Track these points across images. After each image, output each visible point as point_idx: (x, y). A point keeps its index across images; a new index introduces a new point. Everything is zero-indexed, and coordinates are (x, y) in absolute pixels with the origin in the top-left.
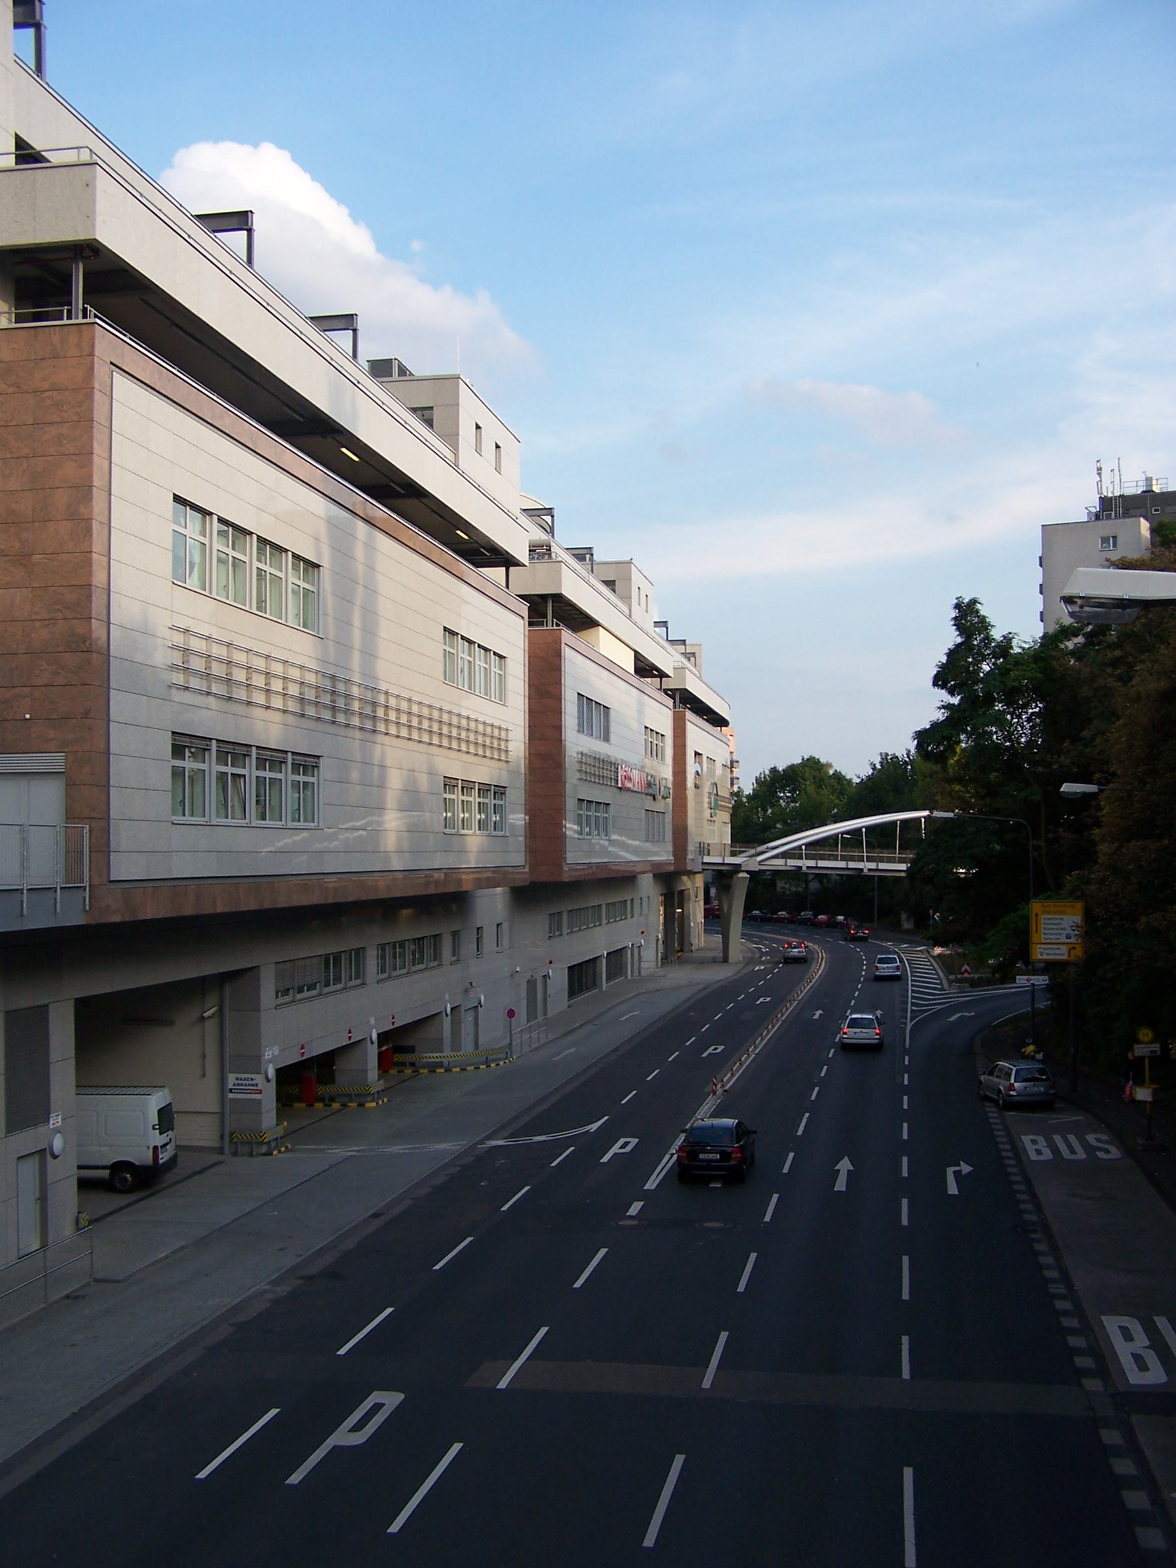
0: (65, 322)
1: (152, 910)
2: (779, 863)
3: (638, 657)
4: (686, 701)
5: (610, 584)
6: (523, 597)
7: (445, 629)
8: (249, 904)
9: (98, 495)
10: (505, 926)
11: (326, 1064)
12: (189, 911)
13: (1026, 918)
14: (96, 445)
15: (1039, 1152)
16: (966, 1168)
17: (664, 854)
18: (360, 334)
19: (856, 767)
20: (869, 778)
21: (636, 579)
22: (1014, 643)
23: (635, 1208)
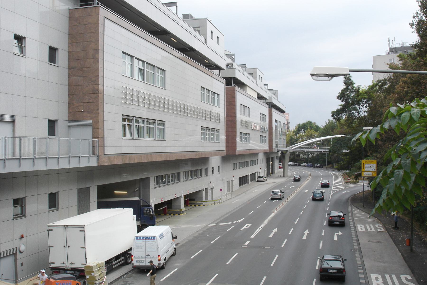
0: (92, 6)
1: (117, 162)
2: (299, 150)
3: (258, 94)
4: (272, 106)
5: (251, 74)
6: (225, 78)
7: (201, 87)
8: (144, 160)
9: (101, 52)
10: (220, 167)
11: (170, 203)
12: (127, 162)
13: (361, 164)
14: (100, 39)
15: (361, 229)
16: (340, 233)
17: (266, 147)
18: (178, 7)
19: (322, 123)
20: (325, 126)
21: (259, 73)
22: (361, 88)
23: (247, 243)
